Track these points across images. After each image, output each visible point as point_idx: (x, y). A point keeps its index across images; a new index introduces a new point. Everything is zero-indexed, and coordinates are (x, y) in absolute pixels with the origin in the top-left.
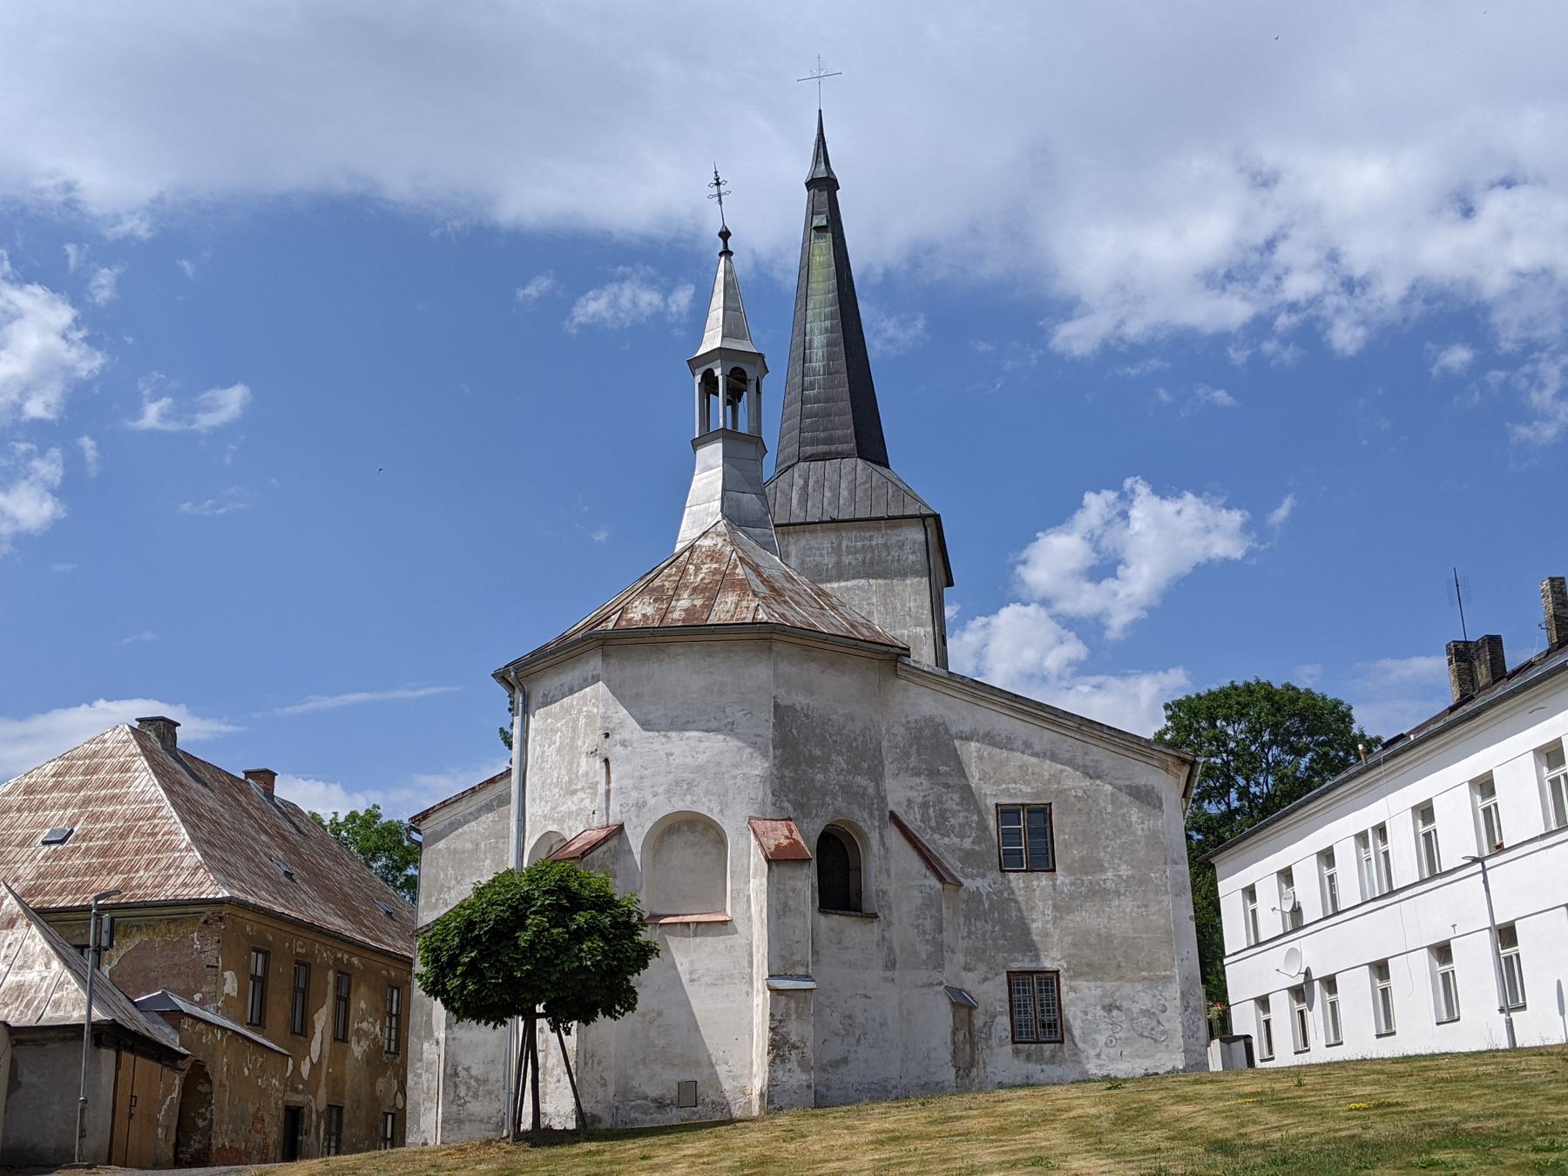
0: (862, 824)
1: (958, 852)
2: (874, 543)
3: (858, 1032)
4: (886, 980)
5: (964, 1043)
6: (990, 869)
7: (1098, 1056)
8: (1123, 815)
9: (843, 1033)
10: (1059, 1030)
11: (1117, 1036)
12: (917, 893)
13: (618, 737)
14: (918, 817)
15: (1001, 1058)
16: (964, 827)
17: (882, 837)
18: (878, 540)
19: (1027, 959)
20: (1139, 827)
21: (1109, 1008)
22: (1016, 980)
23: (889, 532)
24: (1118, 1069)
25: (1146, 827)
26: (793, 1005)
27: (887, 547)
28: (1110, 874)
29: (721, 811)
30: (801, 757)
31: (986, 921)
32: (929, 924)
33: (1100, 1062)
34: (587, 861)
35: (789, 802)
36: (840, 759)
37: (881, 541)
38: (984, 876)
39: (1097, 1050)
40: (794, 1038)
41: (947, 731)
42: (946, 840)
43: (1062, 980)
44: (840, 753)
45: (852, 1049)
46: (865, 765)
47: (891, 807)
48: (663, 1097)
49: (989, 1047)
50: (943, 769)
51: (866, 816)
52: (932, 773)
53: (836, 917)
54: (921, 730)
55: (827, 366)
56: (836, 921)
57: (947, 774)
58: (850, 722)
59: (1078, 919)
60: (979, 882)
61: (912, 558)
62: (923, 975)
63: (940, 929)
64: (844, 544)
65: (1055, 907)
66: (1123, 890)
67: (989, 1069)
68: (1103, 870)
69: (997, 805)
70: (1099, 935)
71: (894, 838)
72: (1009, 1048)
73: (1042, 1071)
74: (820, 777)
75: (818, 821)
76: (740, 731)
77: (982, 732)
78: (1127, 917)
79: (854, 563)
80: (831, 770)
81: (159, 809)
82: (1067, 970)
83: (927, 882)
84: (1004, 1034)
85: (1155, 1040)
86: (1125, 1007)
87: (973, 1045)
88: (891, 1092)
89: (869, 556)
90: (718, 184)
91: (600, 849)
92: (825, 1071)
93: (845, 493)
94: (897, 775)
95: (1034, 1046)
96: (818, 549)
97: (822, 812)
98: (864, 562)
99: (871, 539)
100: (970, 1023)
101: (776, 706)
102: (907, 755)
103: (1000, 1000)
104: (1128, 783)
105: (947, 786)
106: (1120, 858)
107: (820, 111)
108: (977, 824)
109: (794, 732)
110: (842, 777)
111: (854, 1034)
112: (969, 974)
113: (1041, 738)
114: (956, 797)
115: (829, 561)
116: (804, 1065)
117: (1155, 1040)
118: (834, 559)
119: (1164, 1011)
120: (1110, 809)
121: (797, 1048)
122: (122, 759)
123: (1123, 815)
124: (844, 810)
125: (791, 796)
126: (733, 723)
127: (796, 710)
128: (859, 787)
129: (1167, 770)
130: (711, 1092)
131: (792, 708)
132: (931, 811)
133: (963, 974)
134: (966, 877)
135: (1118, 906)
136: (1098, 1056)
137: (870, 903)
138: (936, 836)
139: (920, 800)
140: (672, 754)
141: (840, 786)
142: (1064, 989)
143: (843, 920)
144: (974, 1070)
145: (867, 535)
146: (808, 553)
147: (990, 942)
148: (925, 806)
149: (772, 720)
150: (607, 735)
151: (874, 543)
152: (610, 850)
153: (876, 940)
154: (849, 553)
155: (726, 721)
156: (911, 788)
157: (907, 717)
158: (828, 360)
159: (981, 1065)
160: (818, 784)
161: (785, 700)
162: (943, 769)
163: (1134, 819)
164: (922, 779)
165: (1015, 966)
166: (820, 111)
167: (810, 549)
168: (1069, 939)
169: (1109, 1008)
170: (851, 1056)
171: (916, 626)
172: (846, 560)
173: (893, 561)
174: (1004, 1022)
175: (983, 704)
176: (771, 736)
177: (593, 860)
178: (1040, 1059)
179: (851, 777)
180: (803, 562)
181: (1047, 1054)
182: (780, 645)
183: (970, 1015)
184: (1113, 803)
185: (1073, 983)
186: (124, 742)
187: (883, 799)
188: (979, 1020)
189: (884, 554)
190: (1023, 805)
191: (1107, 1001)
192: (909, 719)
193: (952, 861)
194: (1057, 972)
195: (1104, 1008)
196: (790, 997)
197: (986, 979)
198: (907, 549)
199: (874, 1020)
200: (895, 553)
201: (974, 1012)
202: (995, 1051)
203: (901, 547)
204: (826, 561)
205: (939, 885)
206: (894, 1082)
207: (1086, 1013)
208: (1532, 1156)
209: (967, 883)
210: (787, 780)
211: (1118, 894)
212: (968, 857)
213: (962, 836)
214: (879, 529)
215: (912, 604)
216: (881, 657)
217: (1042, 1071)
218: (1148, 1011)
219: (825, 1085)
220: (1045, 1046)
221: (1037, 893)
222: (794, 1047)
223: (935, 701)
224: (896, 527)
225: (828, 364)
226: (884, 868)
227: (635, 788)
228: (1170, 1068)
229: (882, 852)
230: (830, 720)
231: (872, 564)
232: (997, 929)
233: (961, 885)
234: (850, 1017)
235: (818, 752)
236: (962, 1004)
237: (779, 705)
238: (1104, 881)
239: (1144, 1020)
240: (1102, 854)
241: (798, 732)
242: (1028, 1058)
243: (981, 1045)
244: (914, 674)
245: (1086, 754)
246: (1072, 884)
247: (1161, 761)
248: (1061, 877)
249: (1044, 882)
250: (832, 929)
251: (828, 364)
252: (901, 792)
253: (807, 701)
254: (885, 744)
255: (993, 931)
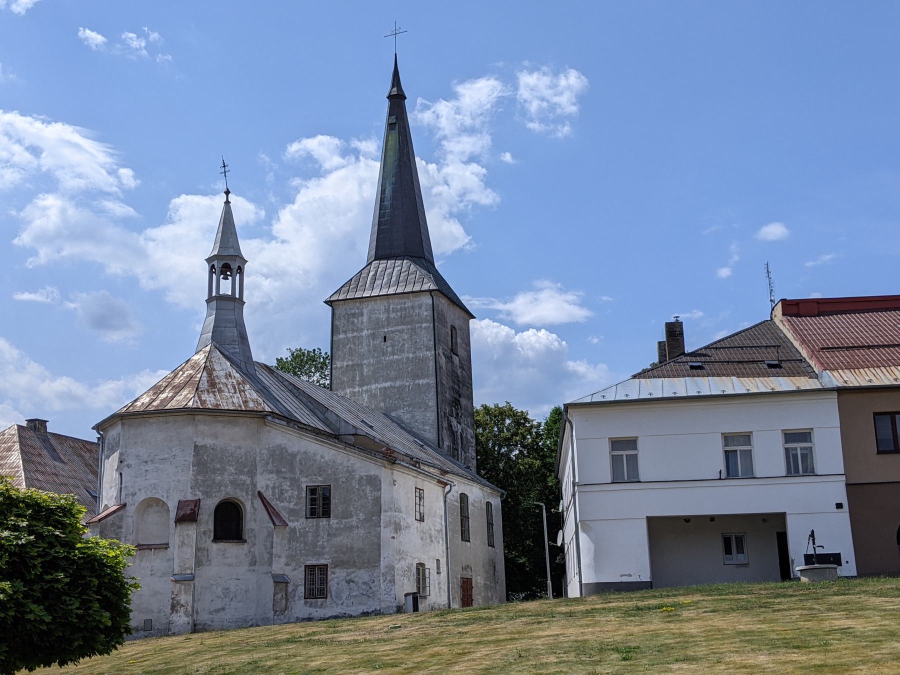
0: (241, 498)
1: (287, 510)
2: (406, 306)
3: (231, 596)
4: (250, 571)
5: (281, 599)
6: (301, 517)
7: (342, 604)
8: (363, 490)
9: (223, 596)
10: (325, 592)
11: (351, 595)
12: (265, 530)
13: (126, 463)
14: (270, 493)
15: (300, 607)
16: (116, 534)
17: (252, 503)
18: (409, 304)
19: (314, 559)
20: (370, 495)
21: (349, 582)
22: (310, 569)
23: (414, 299)
24: (350, 610)
25: (373, 495)
26: (183, 587)
27: (413, 307)
28: (354, 518)
29: (167, 497)
30: (208, 470)
31: (297, 542)
32: (269, 544)
33: (343, 607)
34: (102, 523)
35: (199, 491)
36: (231, 468)
37: (410, 304)
38: (298, 521)
39: (342, 601)
40: (182, 602)
41: (286, 451)
42: (282, 504)
43: (329, 569)
44: (231, 465)
45: (228, 604)
46: (246, 470)
47: (259, 489)
48: (138, 626)
49: (294, 601)
50: (283, 470)
51: (244, 494)
52: (279, 472)
53: (222, 543)
54: (275, 451)
55: (392, 204)
56: (222, 545)
57: (285, 472)
58: (238, 449)
59: (339, 540)
60: (296, 524)
61: (425, 313)
62: (265, 568)
63: (272, 547)
64: (391, 307)
65: (329, 535)
66: (359, 526)
67: (293, 611)
68: (352, 516)
69: (307, 486)
70: (347, 547)
71: (258, 503)
72: (303, 601)
73: (317, 611)
74: (219, 478)
75: (216, 499)
76: (177, 459)
77: (302, 451)
78: (361, 538)
79: (395, 317)
80: (226, 474)
81: (18, 471)
82: (331, 564)
83: (269, 525)
84: (301, 595)
85: (368, 596)
86: (356, 581)
87: (287, 600)
88: (249, 622)
89: (404, 312)
90: (224, 166)
91: (111, 517)
92: (211, 614)
93: (393, 279)
94: (262, 473)
95: (314, 600)
96: (378, 310)
97: (218, 494)
98: (401, 316)
99: (405, 304)
100: (286, 589)
101: (196, 446)
102: (267, 464)
103: (300, 579)
104: (366, 474)
105: (284, 478)
106: (360, 510)
107: (396, 55)
108: (297, 496)
109: (205, 457)
110: (231, 477)
111: (229, 596)
112: (288, 567)
113: (329, 453)
114: (288, 483)
115: (383, 316)
116: (186, 613)
117: (368, 596)
118: (386, 315)
119: (373, 583)
120: (357, 487)
121: (184, 606)
122: (9, 445)
123: (363, 490)
124: (231, 493)
125: (201, 488)
126: (175, 455)
127: (207, 447)
128: (241, 481)
129: (385, 467)
130: (157, 624)
131: (205, 446)
132: (277, 490)
133: (285, 567)
134: (290, 521)
135: (357, 533)
136: (342, 604)
137: (246, 536)
138: (278, 502)
139: (272, 485)
140: (148, 471)
141: (229, 481)
142: (329, 573)
143: (227, 544)
144: (287, 612)
145: (403, 301)
146: (373, 312)
147: (298, 552)
148: (274, 488)
149: (193, 453)
150: (121, 462)
151: (406, 306)
152: (118, 516)
153: (245, 552)
154: (393, 312)
155: (171, 454)
156: (268, 479)
157: (269, 445)
158: (393, 200)
159: (290, 609)
160: (217, 482)
161: (200, 442)
162: (283, 470)
163: (368, 491)
164: (274, 475)
165: (309, 563)
166: (396, 55)
167: (374, 310)
168: (334, 549)
169: (349, 582)
170: (227, 607)
171: (427, 351)
172: (392, 316)
173: (416, 315)
174: (302, 589)
175: (304, 437)
176: (192, 461)
177: (106, 525)
178: (316, 607)
179: (237, 477)
180: (370, 317)
181: (319, 603)
182: (200, 416)
183: (287, 586)
184: (359, 484)
185: (334, 570)
186: (13, 435)
187: (254, 485)
188: (290, 589)
189: (411, 312)
190: (318, 486)
191: (348, 578)
192: (270, 446)
193: (284, 514)
194: (327, 565)
195: (346, 581)
196: (182, 584)
197: (295, 569)
198: (423, 309)
199: (241, 590)
200: (417, 311)
201: (289, 585)
202: (297, 602)
203: (420, 308)
204: (382, 317)
205: (273, 527)
206: (251, 618)
207: (338, 584)
208: (871, 628)
209: (290, 524)
210: (199, 481)
211: (357, 527)
212: (292, 512)
213: (290, 502)
214: (409, 298)
215: (425, 339)
216: (258, 416)
217: (317, 611)
218: (366, 582)
219: (211, 621)
220: (319, 600)
221: (321, 528)
222: (182, 606)
223: (282, 437)
224: (417, 296)
225: (393, 203)
226: (253, 518)
227: (132, 486)
228: (374, 609)
229: (252, 511)
230: (226, 450)
231: (405, 317)
232: (302, 545)
233: (287, 525)
234: (227, 589)
235: (219, 466)
236: (280, 582)
237: (197, 446)
238: (352, 521)
239: (364, 587)
240: (352, 509)
241: (207, 458)
242: (311, 606)
243: (291, 600)
244: (272, 424)
245: (349, 460)
246: (337, 523)
247: (381, 463)
248: (333, 521)
249: (325, 523)
250: (219, 550)
251: (393, 203)
252: (264, 481)
253: (214, 442)
254: (258, 458)
255: (300, 547)
